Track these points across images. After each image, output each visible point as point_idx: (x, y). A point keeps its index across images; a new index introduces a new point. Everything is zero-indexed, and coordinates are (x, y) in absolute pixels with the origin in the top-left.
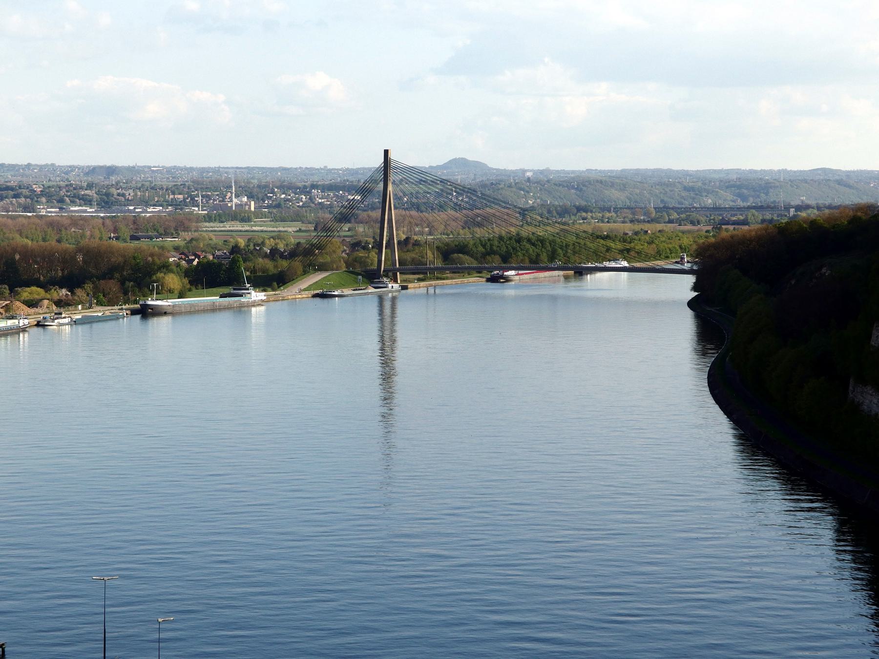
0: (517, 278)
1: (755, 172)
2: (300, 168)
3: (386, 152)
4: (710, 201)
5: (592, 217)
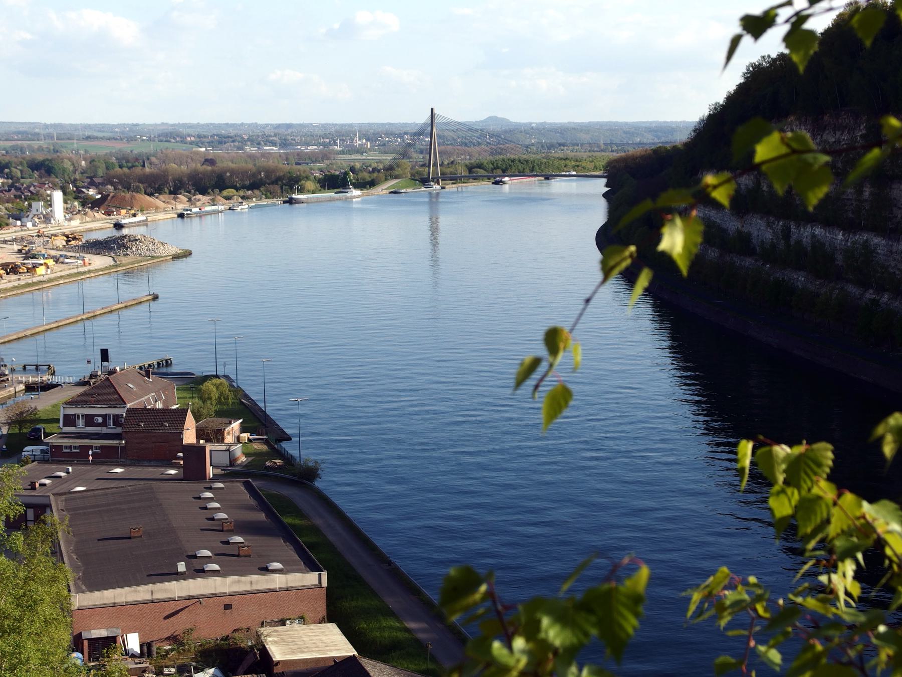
0: (510, 182)
1: (667, 122)
2: (400, 123)
3: (432, 110)
4: (639, 140)
5: (567, 149)
